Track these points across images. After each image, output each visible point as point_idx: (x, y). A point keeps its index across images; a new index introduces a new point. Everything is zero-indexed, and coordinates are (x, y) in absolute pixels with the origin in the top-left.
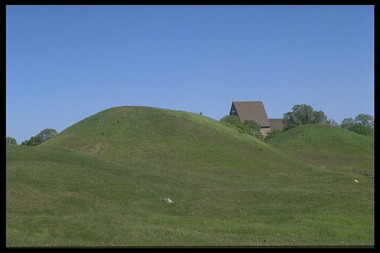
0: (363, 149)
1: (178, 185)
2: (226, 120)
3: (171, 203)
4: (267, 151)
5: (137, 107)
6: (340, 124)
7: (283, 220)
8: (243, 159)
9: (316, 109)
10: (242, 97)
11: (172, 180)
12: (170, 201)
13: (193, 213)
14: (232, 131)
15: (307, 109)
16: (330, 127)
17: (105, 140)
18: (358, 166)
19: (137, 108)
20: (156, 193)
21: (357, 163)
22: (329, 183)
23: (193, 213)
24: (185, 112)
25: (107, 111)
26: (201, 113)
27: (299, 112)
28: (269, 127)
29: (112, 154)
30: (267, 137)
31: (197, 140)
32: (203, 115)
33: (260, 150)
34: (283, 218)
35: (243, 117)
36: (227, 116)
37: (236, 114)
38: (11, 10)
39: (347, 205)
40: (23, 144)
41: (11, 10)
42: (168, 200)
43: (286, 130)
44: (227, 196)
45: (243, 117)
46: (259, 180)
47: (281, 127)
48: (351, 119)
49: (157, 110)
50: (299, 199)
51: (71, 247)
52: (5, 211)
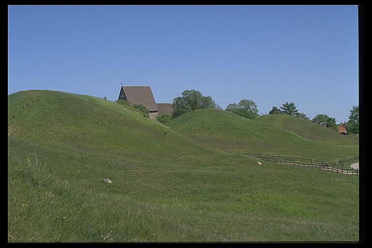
0: (253, 133)
2: (118, 102)
3: (110, 183)
4: (171, 135)
6: (224, 109)
11: (100, 162)
12: (110, 181)
15: (196, 94)
16: (219, 112)
17: (16, 123)
19: (46, 92)
20: (90, 174)
21: (249, 147)
25: (20, 92)
26: (105, 98)
27: (188, 98)
28: (157, 111)
29: (25, 137)
33: (165, 133)
37: (125, 98)
38: (13, 10)
40: (274, 111)
41: (13, 10)
42: (108, 181)
43: (175, 115)
47: (170, 112)
48: (235, 104)
49: (65, 94)
50: (223, 180)
52: (7, 187)
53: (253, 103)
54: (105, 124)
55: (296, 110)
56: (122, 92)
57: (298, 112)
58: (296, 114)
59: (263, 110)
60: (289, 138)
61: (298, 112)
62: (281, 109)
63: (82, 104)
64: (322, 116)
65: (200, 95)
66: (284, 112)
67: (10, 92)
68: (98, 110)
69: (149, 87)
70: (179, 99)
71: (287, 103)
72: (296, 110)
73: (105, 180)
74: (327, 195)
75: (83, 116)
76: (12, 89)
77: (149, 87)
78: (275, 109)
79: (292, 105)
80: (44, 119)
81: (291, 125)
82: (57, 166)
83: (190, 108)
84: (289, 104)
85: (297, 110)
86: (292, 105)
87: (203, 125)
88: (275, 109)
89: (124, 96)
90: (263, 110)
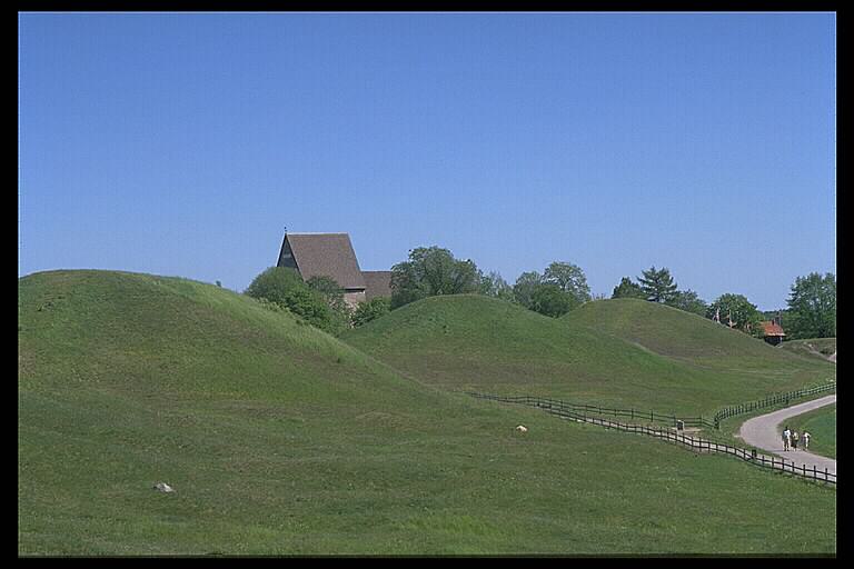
1: (178, 450)
5: (87, 271)
6: (512, 284)
7: (369, 524)
8: (303, 381)
9: (460, 256)
10: (309, 224)
13: (210, 511)
14: (280, 320)
15: (440, 256)
18: (537, 385)
22: (469, 432)
23: (210, 511)
24: (186, 279)
26: (219, 283)
27: (423, 265)
30: (358, 311)
31: (212, 343)
32: (223, 286)
33: (339, 361)
34: (369, 520)
35: (308, 269)
36: (272, 268)
38: (29, 23)
39: (488, 490)
40: (625, 289)
41: (29, 23)
43: (397, 302)
44: (272, 473)
45: (308, 269)
46: (335, 429)
49: (132, 279)
51: (602, 555)
53: (577, 271)
54: (209, 345)
55: (673, 284)
56: (286, 247)
57: (677, 290)
58: (672, 294)
59: (601, 286)
60: (630, 357)
61: (677, 290)
62: (639, 283)
63: (165, 300)
64: (733, 298)
65: (450, 258)
66: (647, 289)
67: (23, 271)
68: (197, 314)
69: (347, 235)
70: (404, 265)
71: (653, 269)
72: (673, 284)
73: (159, 486)
74: (591, 511)
75: (165, 326)
76: (29, 263)
77: (347, 235)
78: (626, 281)
79: (664, 273)
80: (83, 335)
81: (650, 323)
82: (74, 454)
83: (428, 288)
84: (657, 271)
85: (675, 287)
86: (664, 273)
87: (442, 331)
88: (626, 281)
89: (290, 256)
90: (601, 286)
